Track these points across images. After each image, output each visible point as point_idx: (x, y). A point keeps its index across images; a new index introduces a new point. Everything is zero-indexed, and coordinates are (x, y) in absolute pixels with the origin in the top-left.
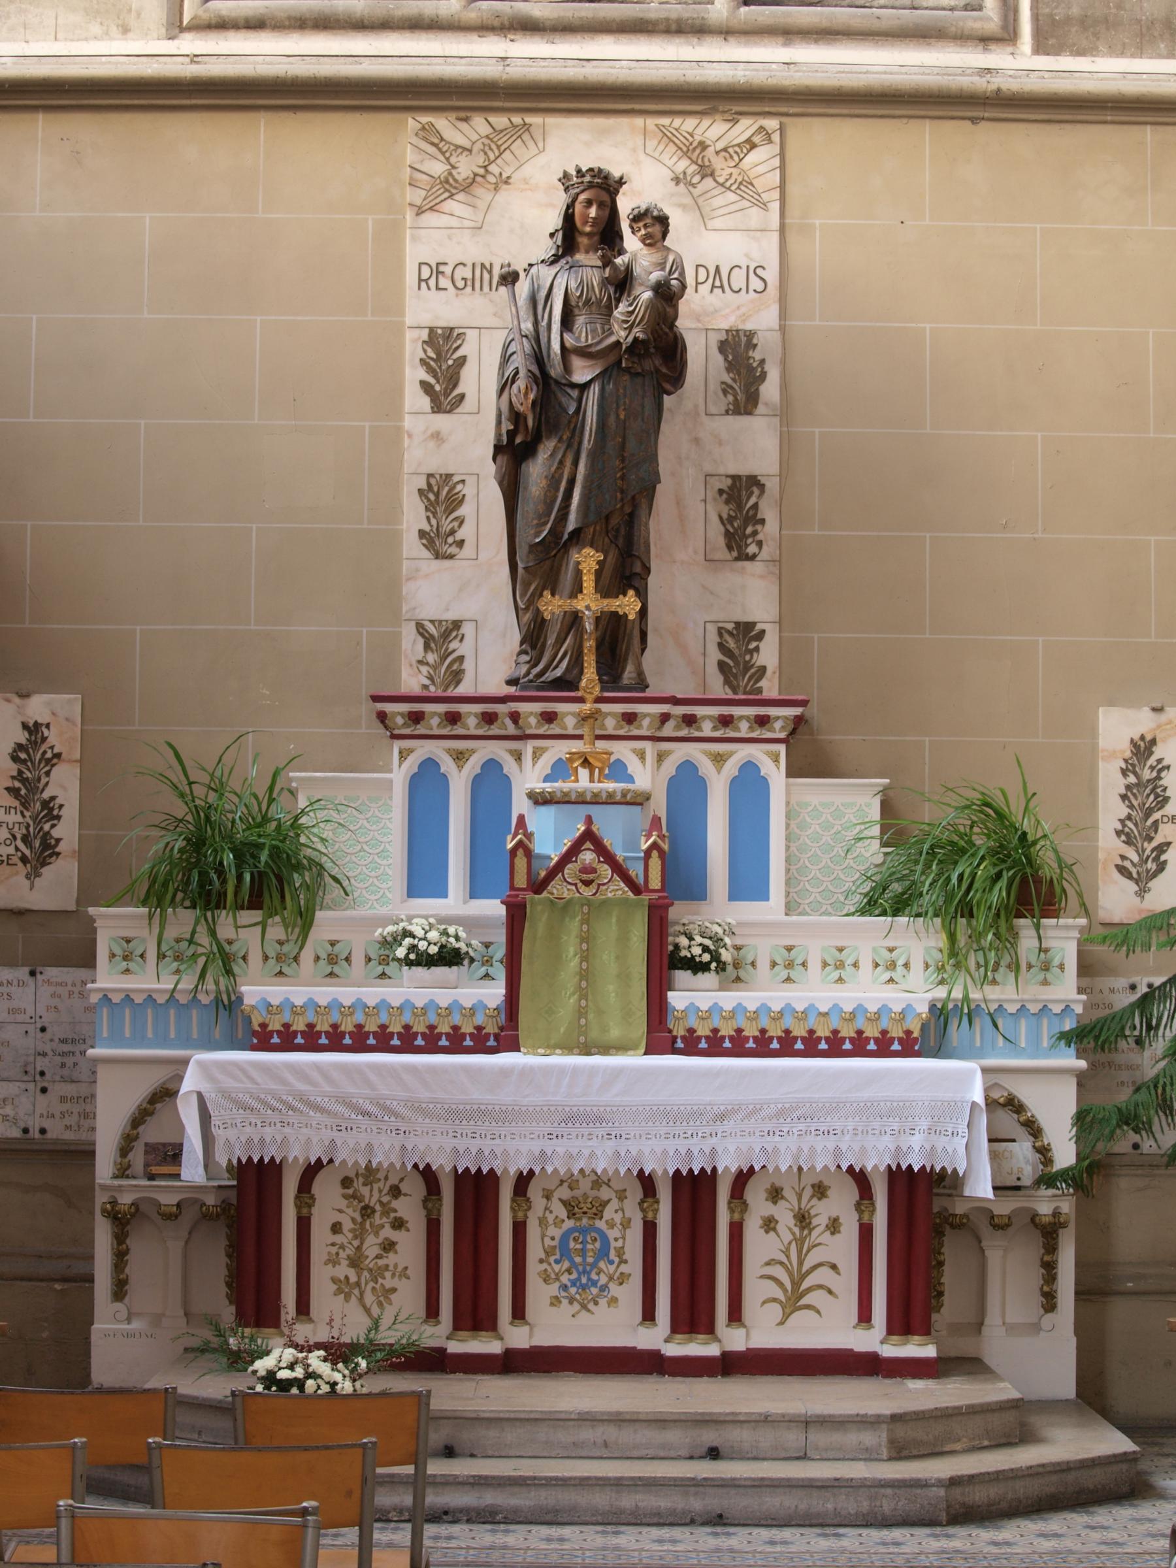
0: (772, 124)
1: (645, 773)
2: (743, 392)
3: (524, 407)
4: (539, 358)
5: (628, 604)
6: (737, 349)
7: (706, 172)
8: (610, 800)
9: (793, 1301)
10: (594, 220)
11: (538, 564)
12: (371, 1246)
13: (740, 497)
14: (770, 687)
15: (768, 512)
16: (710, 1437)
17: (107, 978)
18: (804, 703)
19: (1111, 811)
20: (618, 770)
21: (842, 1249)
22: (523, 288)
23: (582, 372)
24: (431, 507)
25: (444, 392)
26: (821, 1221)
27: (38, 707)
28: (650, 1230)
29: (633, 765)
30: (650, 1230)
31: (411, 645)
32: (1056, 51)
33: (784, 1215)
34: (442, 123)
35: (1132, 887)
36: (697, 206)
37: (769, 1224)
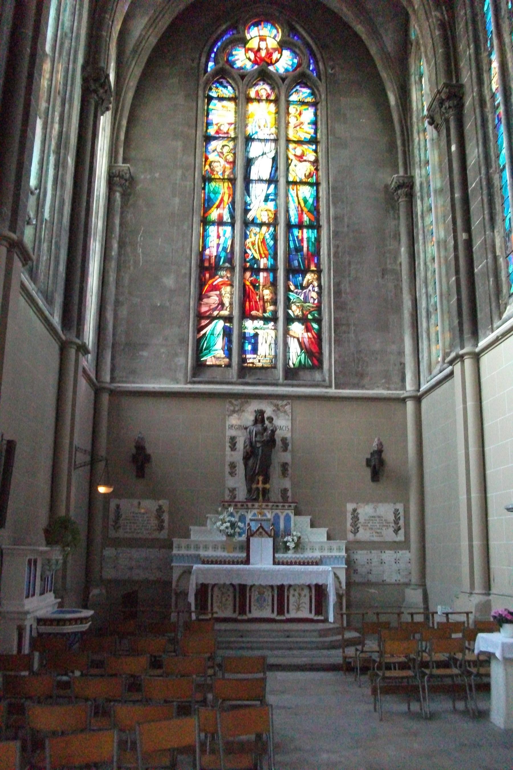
0: (290, 401)
1: (269, 515)
2: (285, 449)
3: (249, 451)
4: (251, 443)
5: (267, 486)
6: (284, 440)
7: (278, 409)
8: (264, 520)
9: (298, 609)
10: (260, 418)
11: (250, 479)
12: (224, 599)
13: (284, 467)
14: (290, 500)
15: (289, 469)
16: (287, 634)
17: (175, 552)
18: (297, 503)
19: (349, 521)
20: (265, 515)
21: (307, 600)
22: (248, 430)
23: (258, 445)
24: (231, 468)
25: (233, 447)
26: (303, 595)
27: (161, 502)
28: (273, 597)
29: (267, 514)
30: (273, 597)
31: (227, 492)
32: (339, 389)
33: (296, 594)
34: (233, 401)
35: (353, 535)
36: (277, 415)
37: (294, 595)
